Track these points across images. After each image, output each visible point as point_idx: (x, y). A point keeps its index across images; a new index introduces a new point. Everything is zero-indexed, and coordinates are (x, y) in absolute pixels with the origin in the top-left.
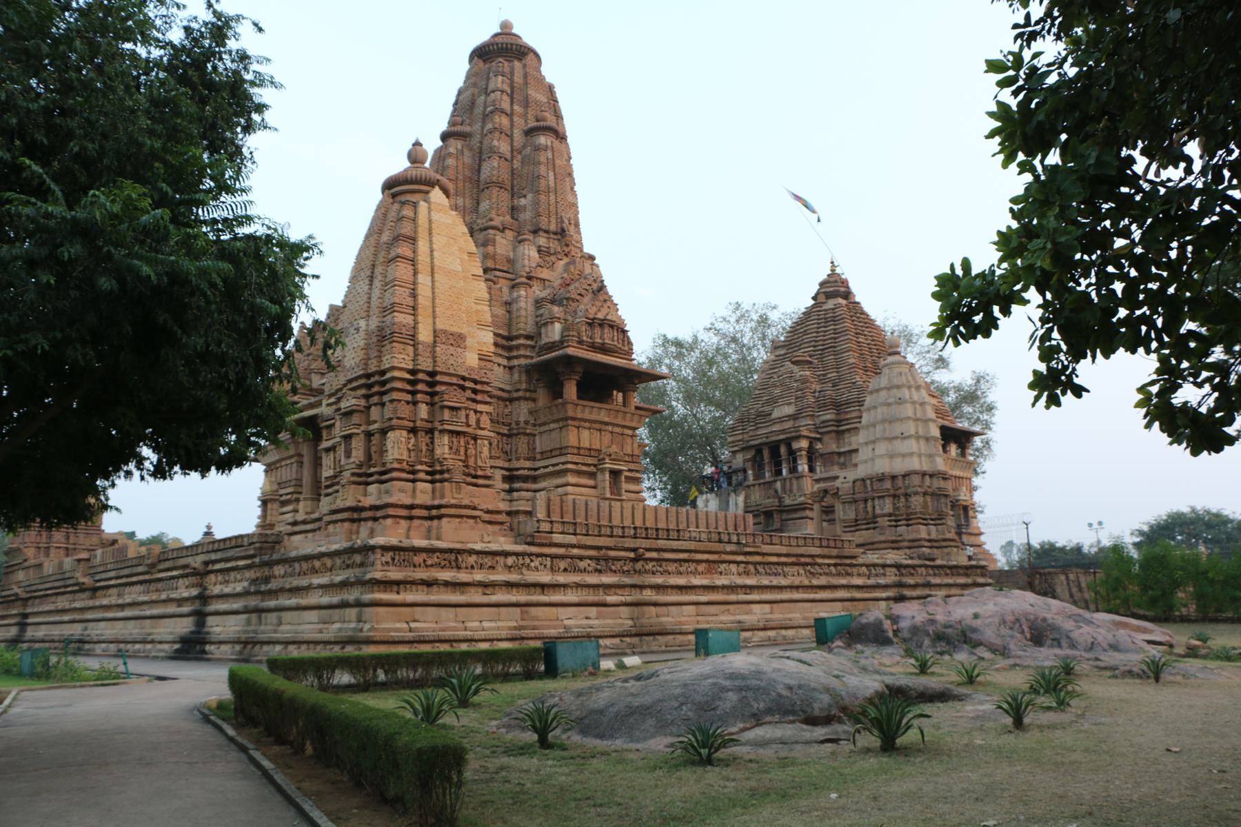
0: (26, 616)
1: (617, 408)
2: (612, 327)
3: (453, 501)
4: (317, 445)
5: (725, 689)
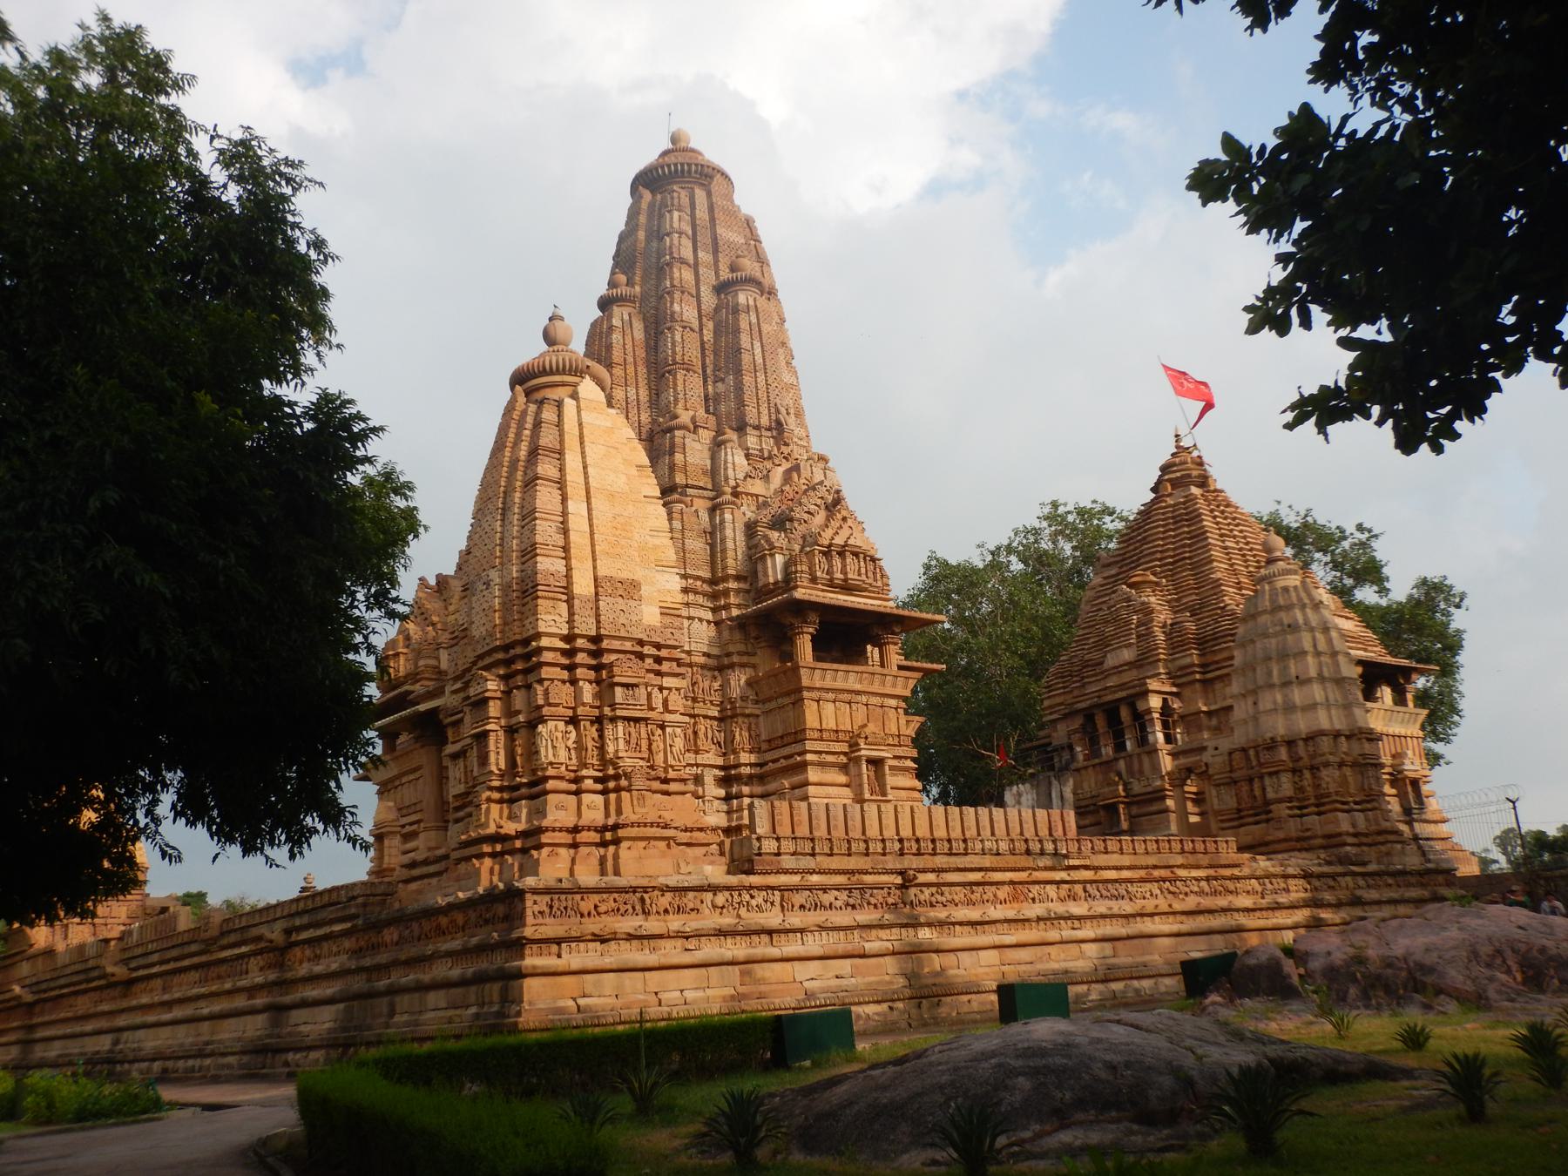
0: (31, 1028)
1: (870, 669)
2: (856, 554)
3: (634, 818)
4: (440, 751)
5: (1014, 1073)
